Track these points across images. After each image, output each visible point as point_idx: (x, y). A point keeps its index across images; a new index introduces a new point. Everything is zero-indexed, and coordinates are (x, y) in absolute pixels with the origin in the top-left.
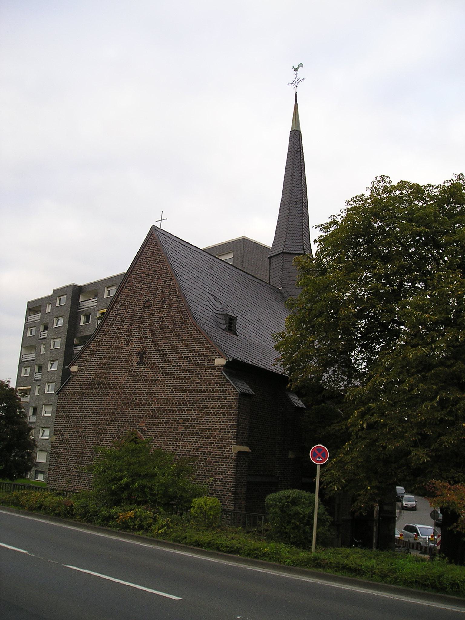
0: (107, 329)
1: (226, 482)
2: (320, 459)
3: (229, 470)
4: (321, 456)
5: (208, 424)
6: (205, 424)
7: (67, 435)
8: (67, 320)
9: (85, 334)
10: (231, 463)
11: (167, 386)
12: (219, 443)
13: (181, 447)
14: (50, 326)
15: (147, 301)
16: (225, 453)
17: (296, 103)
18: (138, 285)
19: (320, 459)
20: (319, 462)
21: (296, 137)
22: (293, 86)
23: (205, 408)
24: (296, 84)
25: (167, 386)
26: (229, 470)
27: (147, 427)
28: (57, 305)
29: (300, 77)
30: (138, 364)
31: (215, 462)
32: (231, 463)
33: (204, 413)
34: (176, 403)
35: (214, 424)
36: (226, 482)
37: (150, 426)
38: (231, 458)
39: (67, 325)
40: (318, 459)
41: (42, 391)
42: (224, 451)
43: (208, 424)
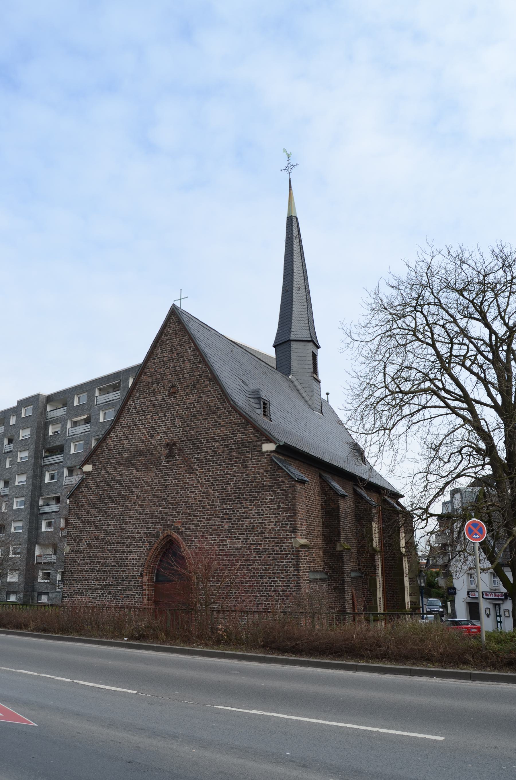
0: (125, 420)
1: (289, 581)
2: (478, 536)
3: (290, 567)
4: (478, 533)
5: (261, 518)
6: (257, 518)
7: (84, 544)
8: (35, 431)
9: (55, 445)
10: (292, 559)
11: (205, 479)
12: (276, 538)
13: (228, 546)
14: (15, 438)
15: (173, 387)
16: (284, 549)
17: (290, 187)
18: (161, 370)
19: (478, 536)
20: (476, 539)
21: (292, 223)
22: (286, 173)
23: (254, 500)
24: (289, 170)
25: (205, 479)
26: (290, 567)
27: (184, 527)
28: (23, 416)
29: (293, 162)
30: (167, 457)
31: (273, 560)
32: (292, 559)
33: (254, 505)
34: (218, 497)
35: (267, 517)
36: (289, 581)
37: (188, 525)
38: (292, 554)
39: (35, 436)
40: (475, 536)
41: (10, 506)
42: (282, 546)
43: (261, 518)
